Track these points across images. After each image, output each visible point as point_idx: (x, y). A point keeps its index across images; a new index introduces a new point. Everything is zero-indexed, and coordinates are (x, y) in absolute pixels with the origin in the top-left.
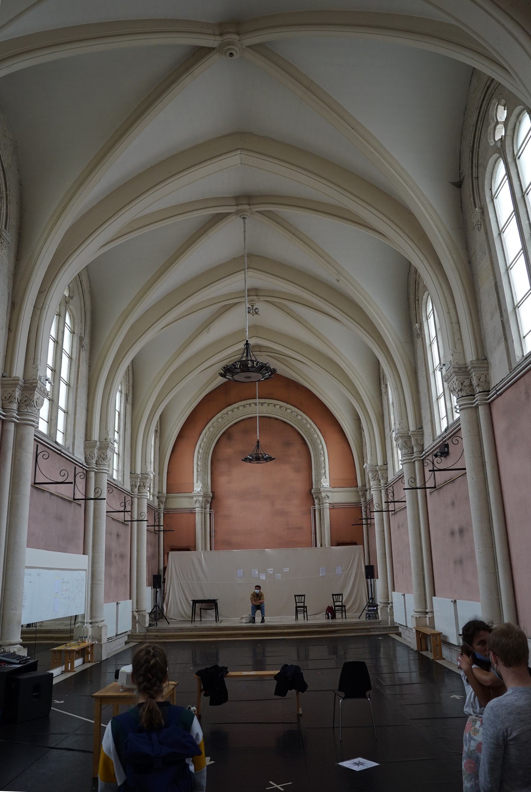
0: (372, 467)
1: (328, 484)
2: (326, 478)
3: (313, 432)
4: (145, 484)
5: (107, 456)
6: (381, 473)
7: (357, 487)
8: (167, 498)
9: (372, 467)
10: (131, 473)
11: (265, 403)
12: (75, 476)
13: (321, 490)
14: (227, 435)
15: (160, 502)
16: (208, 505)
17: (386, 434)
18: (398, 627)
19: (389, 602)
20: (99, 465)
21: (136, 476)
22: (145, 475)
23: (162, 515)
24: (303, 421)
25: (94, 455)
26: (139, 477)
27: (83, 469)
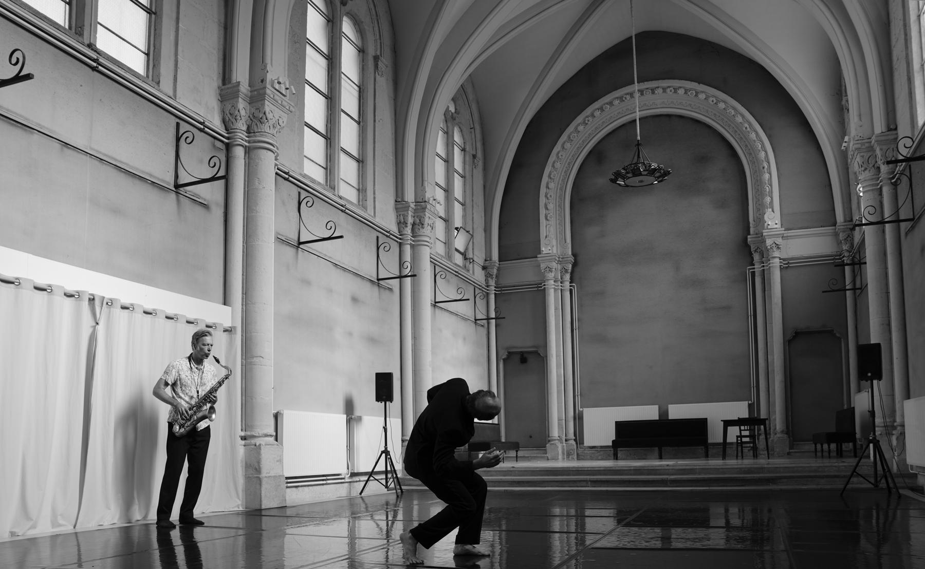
0: (860, 142)
1: (778, 221)
2: (773, 211)
3: (749, 129)
4: (422, 219)
5: (265, 113)
6: (881, 149)
7: (835, 224)
8: (499, 269)
9: (860, 142)
10: (396, 201)
11: (658, 87)
12: (475, 297)
13: (764, 234)
14: (597, 155)
15: (488, 275)
16: (567, 277)
17: (895, 58)
18: (916, 474)
19: (895, 424)
20: (252, 134)
21: (404, 206)
22: (422, 204)
23: (492, 297)
24: (728, 111)
25: (237, 112)
26: (495, 266)
27: (483, 291)
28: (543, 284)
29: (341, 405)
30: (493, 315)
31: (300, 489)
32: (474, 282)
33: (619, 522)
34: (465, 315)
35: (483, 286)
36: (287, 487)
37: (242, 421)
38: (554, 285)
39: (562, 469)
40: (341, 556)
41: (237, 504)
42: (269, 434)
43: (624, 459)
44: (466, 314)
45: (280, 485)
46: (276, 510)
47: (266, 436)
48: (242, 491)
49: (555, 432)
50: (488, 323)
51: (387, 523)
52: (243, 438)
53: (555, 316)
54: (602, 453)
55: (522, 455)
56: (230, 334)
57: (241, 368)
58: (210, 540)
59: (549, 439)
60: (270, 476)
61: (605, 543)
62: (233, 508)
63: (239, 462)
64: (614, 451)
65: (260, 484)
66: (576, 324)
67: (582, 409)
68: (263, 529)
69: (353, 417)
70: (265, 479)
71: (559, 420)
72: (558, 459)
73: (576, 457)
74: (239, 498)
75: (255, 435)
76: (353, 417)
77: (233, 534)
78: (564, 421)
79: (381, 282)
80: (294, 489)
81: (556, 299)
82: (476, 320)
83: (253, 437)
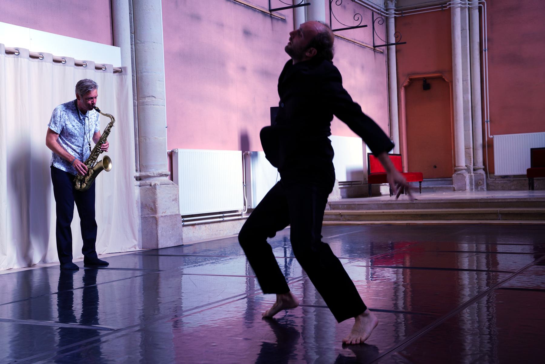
12: (373, 23)
23: (392, 21)
27: (382, 15)
28: (448, 3)
29: (236, 141)
30: (393, 40)
31: (197, 227)
32: (372, 7)
33: (536, 257)
34: (363, 42)
35: (382, 10)
36: (184, 226)
37: (136, 162)
38: (461, 3)
39: (469, 201)
40: (237, 296)
41: (134, 244)
42: (163, 174)
43: (541, 189)
44: (364, 42)
45: (176, 224)
46: (173, 249)
47: (162, 175)
48: (139, 231)
49: (462, 161)
50: (388, 50)
51: (286, 260)
52: (138, 178)
53: (461, 37)
54: (515, 182)
55: (426, 186)
56: (120, 75)
57: (134, 108)
58: (107, 283)
59: (455, 168)
60: (166, 216)
61: (515, 282)
62: (130, 248)
63: (135, 202)
64: (529, 181)
65: (157, 224)
66: (485, 45)
67: (492, 136)
68: (161, 269)
69: (249, 152)
70: (161, 219)
71: (466, 149)
72: (466, 190)
73: (485, 187)
74: (135, 239)
75: (150, 175)
76: (249, 152)
77: (130, 276)
78: (472, 150)
79: (274, 13)
80: (191, 227)
81: (463, 19)
82: (375, 47)
83: (148, 177)
